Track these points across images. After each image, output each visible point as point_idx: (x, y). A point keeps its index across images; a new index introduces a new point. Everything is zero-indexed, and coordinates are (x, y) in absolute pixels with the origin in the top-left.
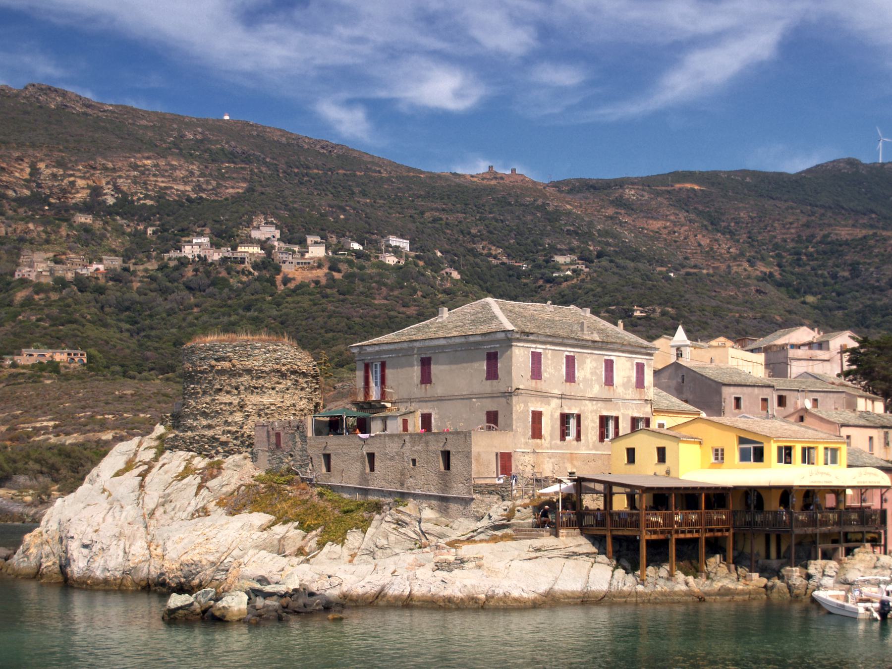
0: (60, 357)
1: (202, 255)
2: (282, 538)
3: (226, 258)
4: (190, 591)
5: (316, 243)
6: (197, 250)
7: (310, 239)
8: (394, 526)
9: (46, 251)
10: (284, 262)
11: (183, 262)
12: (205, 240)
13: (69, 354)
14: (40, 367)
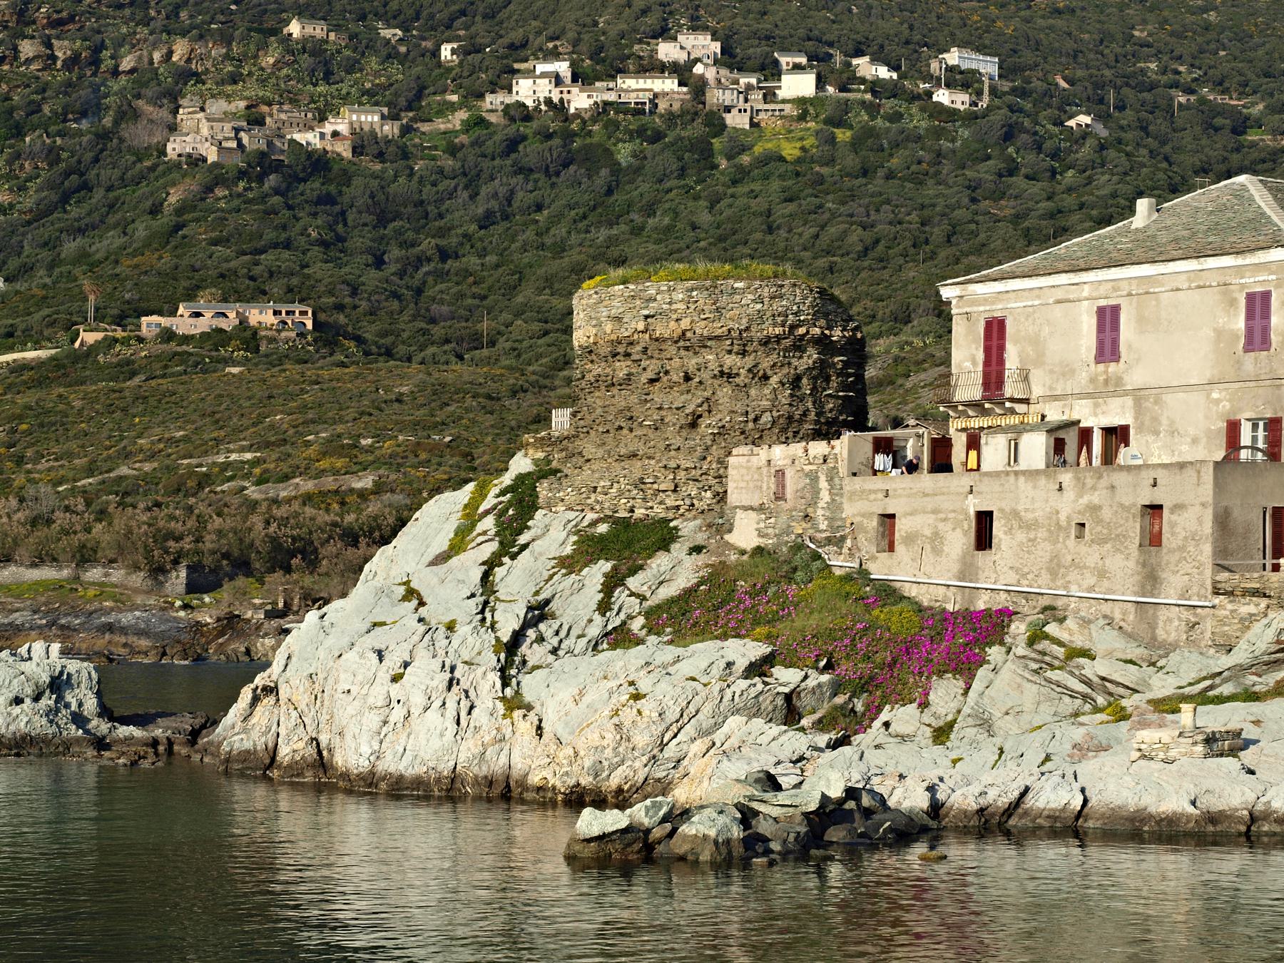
0: (261, 316)
1: (556, 100)
2: (792, 692)
3: (606, 103)
4: (621, 800)
5: (797, 68)
6: (545, 89)
7: (785, 60)
8: (1035, 666)
9: (229, 98)
10: (728, 109)
11: (519, 113)
12: (563, 67)
13: (276, 313)
14: (217, 337)
